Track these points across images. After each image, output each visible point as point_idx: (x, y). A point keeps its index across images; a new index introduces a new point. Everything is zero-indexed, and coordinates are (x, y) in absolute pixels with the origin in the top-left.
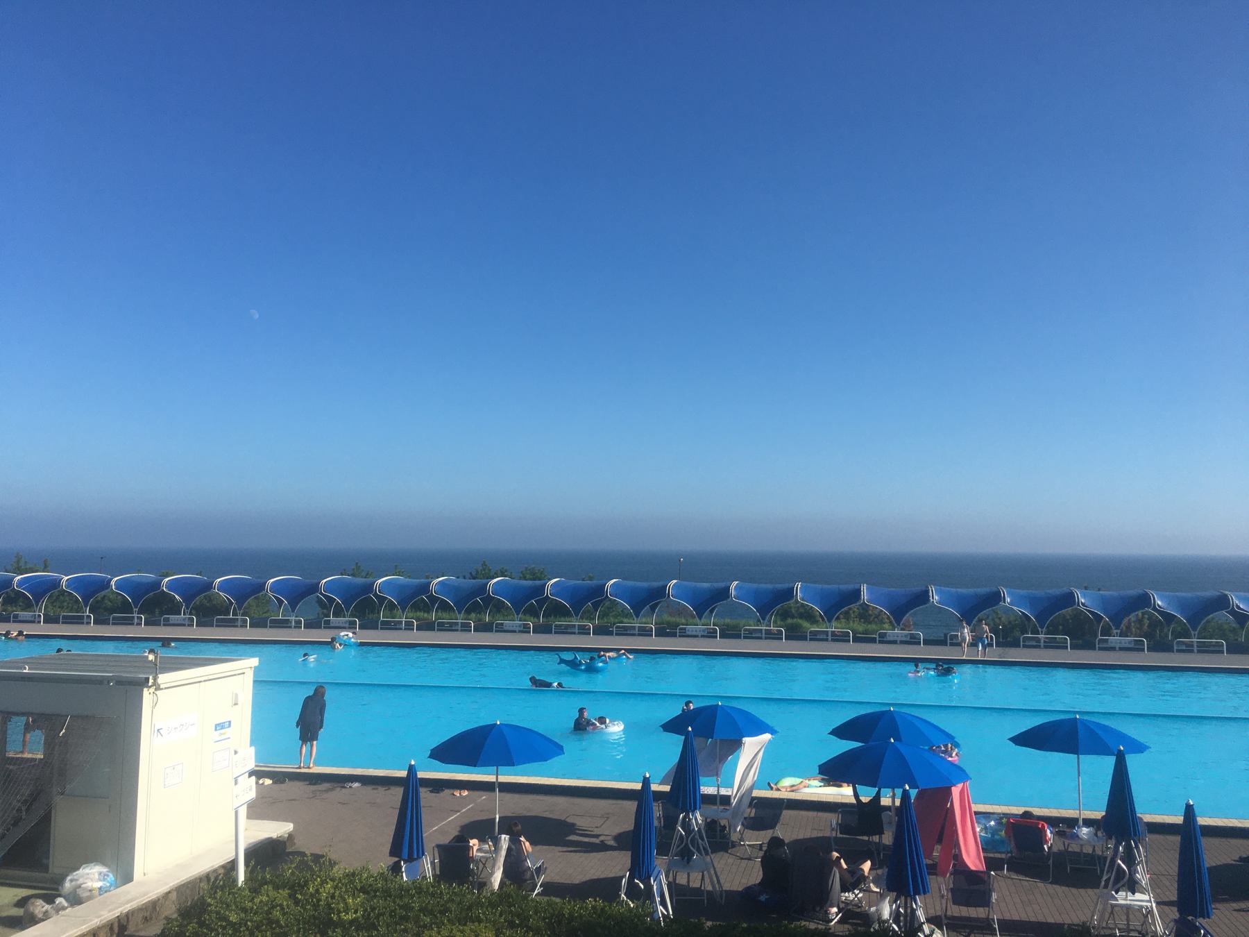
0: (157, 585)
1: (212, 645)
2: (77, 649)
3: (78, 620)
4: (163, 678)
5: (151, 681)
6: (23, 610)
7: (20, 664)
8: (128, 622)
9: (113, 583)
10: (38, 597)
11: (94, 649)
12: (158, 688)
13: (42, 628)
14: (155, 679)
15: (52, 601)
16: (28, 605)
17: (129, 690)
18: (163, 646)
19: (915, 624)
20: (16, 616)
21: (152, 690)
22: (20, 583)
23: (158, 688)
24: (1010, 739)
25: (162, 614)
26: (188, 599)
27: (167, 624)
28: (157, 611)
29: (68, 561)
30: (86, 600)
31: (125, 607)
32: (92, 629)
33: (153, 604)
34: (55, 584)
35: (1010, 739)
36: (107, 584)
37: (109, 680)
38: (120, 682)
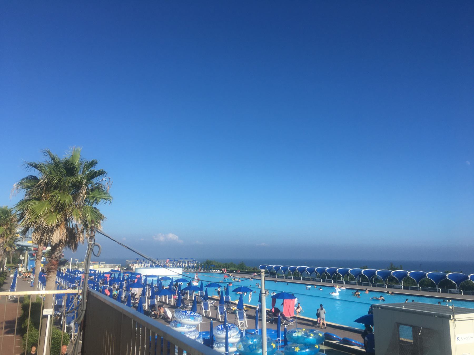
0: (444, 276)
1: (469, 303)
2: (417, 300)
3: (416, 289)
4: (457, 316)
5: (452, 317)
6: (396, 284)
7: (401, 305)
8: (435, 291)
9: (427, 275)
10: (400, 279)
11: (425, 301)
12: (455, 320)
13: (403, 291)
14: (453, 316)
15: (405, 281)
16: (397, 282)
17: (444, 320)
18: (444, 301)
19: (378, 307)
20: (393, 286)
21: (453, 321)
22: (394, 273)
23: (455, 320)
24: (356, 321)
25: (448, 288)
26: (458, 283)
27: (451, 292)
28: (446, 287)
29: (410, 266)
30: (417, 281)
31: (432, 285)
32: (421, 293)
33: (444, 284)
34: (406, 275)
35: (356, 321)
36: (425, 276)
37: (435, 315)
38: (440, 316)
